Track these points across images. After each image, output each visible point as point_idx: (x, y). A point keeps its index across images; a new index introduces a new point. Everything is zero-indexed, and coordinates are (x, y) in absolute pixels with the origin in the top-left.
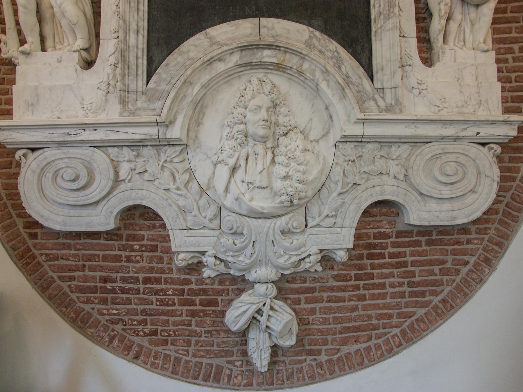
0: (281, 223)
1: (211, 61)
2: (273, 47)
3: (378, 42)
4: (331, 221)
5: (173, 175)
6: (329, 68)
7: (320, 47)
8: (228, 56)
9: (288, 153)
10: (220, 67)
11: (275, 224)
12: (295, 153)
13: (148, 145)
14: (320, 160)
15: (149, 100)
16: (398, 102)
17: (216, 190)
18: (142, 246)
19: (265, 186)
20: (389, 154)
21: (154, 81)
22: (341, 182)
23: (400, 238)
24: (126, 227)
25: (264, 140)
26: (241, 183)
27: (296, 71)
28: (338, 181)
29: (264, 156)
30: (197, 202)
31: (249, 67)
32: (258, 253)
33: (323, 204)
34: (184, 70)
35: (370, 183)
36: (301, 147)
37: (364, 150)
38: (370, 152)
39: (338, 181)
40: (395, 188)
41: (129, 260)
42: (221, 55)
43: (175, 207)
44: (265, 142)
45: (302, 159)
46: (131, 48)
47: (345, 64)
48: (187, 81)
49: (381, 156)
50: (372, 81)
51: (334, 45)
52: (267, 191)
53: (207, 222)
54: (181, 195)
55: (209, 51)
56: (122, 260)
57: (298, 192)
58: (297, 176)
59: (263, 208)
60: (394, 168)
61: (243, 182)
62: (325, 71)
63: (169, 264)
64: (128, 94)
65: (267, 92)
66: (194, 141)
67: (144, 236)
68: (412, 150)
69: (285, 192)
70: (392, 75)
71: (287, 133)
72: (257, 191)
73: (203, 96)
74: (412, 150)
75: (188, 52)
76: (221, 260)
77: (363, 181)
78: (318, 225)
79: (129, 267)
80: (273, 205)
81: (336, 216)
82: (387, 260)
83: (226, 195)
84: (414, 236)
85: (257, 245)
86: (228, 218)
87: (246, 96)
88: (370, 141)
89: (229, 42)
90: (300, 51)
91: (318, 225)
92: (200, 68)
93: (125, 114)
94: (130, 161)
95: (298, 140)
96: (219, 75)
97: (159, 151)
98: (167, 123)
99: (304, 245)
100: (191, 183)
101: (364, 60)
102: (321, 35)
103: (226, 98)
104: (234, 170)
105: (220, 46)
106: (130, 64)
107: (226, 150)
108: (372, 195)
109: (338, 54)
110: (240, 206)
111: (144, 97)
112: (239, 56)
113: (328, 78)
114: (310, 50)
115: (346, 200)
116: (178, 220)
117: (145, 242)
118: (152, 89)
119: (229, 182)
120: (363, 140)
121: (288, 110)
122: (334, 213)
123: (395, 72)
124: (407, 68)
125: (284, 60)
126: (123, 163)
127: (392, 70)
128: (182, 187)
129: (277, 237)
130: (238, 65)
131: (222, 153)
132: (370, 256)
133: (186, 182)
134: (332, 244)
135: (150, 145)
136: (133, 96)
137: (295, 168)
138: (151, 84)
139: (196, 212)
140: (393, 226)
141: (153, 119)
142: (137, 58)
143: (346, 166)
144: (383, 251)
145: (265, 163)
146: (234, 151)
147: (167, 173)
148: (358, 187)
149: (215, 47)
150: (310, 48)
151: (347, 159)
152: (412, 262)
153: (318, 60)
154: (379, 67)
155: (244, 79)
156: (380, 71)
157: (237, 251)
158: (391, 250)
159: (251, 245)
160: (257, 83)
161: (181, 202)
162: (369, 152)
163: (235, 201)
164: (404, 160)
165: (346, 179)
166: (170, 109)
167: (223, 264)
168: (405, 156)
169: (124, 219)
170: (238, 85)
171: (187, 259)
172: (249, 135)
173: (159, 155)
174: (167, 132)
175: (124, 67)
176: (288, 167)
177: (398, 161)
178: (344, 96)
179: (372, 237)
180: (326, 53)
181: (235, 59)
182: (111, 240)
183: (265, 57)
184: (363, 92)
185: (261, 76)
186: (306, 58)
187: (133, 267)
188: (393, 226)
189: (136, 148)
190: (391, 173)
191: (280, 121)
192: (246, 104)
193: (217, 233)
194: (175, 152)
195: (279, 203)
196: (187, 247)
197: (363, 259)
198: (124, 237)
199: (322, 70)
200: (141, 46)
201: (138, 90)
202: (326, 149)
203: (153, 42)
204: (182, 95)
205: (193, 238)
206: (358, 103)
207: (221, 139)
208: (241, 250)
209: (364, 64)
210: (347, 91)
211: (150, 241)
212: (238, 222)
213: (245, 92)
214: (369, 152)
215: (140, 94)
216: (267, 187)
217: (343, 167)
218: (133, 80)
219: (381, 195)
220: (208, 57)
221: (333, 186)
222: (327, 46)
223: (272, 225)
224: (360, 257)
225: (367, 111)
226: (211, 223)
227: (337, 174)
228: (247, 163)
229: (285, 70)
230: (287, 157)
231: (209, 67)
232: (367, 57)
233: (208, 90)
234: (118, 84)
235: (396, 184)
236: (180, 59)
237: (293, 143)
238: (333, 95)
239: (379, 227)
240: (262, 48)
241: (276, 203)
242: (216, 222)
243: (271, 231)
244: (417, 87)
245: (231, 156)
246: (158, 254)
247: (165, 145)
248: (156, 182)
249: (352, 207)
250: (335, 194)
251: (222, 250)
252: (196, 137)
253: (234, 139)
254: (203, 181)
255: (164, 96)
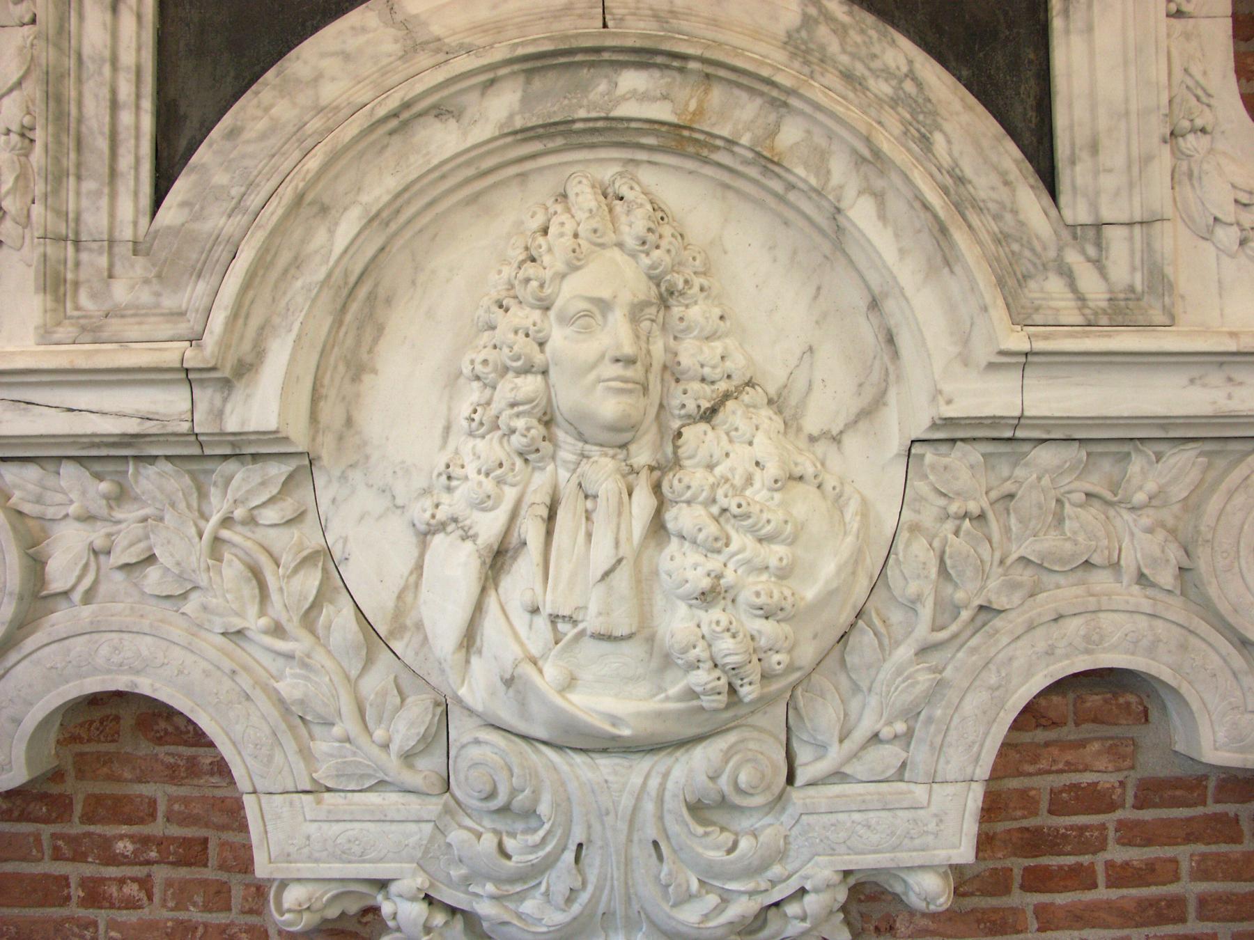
0: (691, 769)
1: (405, 115)
2: (659, 60)
3: (1077, 42)
4: (889, 755)
5: (256, 574)
6: (887, 145)
7: (844, 59)
8: (474, 96)
9: (720, 493)
10: (442, 141)
11: (666, 776)
12: (748, 493)
13: (156, 457)
14: (848, 518)
15: (159, 276)
16: (1159, 280)
17: (426, 638)
18: (145, 841)
19: (622, 630)
20: (1118, 485)
21: (180, 198)
22: (929, 603)
23: (1155, 806)
24: (83, 768)
25: (620, 437)
26: (527, 616)
27: (750, 155)
28: (918, 599)
29: (620, 503)
30: (353, 684)
31: (560, 141)
32: (599, 889)
33: (856, 688)
34: (297, 155)
35: (1046, 603)
36: (772, 470)
37: (1019, 472)
38: (1046, 481)
39: (918, 599)
40: (1143, 622)
41: (94, 895)
42: (446, 92)
43: (264, 704)
44: (624, 446)
45: (777, 517)
46: (90, 66)
47: (947, 127)
48: (310, 197)
49: (1088, 495)
50: (1053, 193)
51: (901, 53)
52: (631, 651)
53: (392, 764)
54: (289, 657)
55: (396, 78)
56: (68, 898)
57: (759, 653)
58: (755, 588)
59: (615, 720)
60: (1139, 543)
61: (535, 611)
62: (866, 153)
63: (251, 912)
64: (77, 250)
65: (631, 243)
66: (341, 438)
67: (153, 803)
68: (1209, 466)
69: (705, 655)
70: (1135, 170)
71: (714, 411)
72: (591, 648)
73: (375, 257)
74: (1209, 466)
75: (317, 79)
76: (453, 911)
77: (1016, 598)
78: (838, 776)
79: (95, 924)
80: (654, 705)
81: (909, 734)
82: (1103, 893)
83: (468, 662)
84: (1210, 800)
85: (593, 858)
86: (475, 752)
87: (547, 259)
88: (1045, 436)
89: (480, 40)
90: (765, 72)
91: (838, 776)
92: (360, 146)
93: (61, 333)
94: (88, 518)
95: (760, 439)
96: (441, 171)
97: (201, 477)
98: (226, 372)
99: (781, 855)
100: (328, 610)
101: (1023, 110)
102: (850, 13)
103: (469, 263)
104: (499, 558)
105: (441, 57)
106: (84, 129)
107: (466, 478)
108: (1050, 652)
109: (919, 85)
110: (522, 705)
111: (140, 261)
112: (519, 94)
113: (879, 184)
114: (806, 70)
115: (948, 673)
116: (278, 758)
117: (158, 828)
118: (174, 231)
119: (479, 608)
120: (1020, 434)
121: (717, 312)
122: (900, 727)
123: (1147, 160)
124: (1191, 143)
125: (700, 112)
126: (63, 523)
127: (1135, 153)
128: (293, 626)
129: (674, 828)
130: (515, 133)
131: (449, 489)
132: (1037, 880)
133: (307, 605)
134: (894, 849)
135: (167, 458)
136: (96, 261)
137: (746, 555)
138: (170, 212)
139: (348, 724)
140: (1128, 763)
141: (170, 354)
142: (114, 105)
143: (951, 536)
144: (1085, 859)
145: (623, 536)
146: (500, 482)
147: (232, 569)
148: (998, 622)
149: (424, 60)
150: (806, 63)
151: (954, 508)
152: (1202, 901)
153: (839, 110)
154: (1082, 135)
155: (542, 188)
156: (1085, 155)
157: (512, 880)
158: (1118, 854)
159: (569, 856)
160: (593, 205)
161: (290, 686)
162: (1039, 479)
163: (501, 688)
164: (1176, 508)
165: (949, 589)
166: (238, 313)
167: (459, 924)
168: (1179, 492)
169: (75, 739)
170: (518, 210)
171: (318, 905)
172: (559, 419)
173: (202, 494)
174: (229, 407)
175: (59, 142)
176: (719, 552)
177: (1150, 511)
178: (944, 255)
179: (1044, 805)
180: (871, 82)
181: (502, 107)
182: (24, 817)
183: (624, 98)
184: (1019, 240)
185: (607, 173)
186: (794, 102)
187: (113, 924)
188: (1128, 763)
189: (110, 467)
190: (1128, 561)
191: (686, 360)
192: (548, 291)
193: (433, 807)
194: (263, 484)
195: (681, 698)
196: (317, 861)
197: (1007, 891)
198: (78, 809)
199: (854, 151)
200: (127, 58)
201: (117, 235)
202: (870, 471)
203: (182, 44)
204: (285, 258)
205: (337, 828)
206: (1001, 283)
207: (447, 429)
208: (531, 874)
209: (1020, 125)
210: (960, 237)
211: (180, 824)
212: (516, 770)
213: (541, 240)
214: (1039, 479)
215: (123, 250)
216: (630, 636)
217: (936, 544)
218: (98, 194)
219: (1088, 652)
220: (393, 102)
221: (896, 616)
222: (874, 56)
223: (654, 783)
224: (998, 883)
225: (1038, 318)
226: (411, 766)
227: (915, 571)
228: (549, 533)
229: (705, 152)
230: (715, 510)
231: (396, 141)
232: (1031, 101)
233: (396, 234)
234: (37, 210)
235: (1146, 606)
236: (284, 111)
237: (741, 451)
238: (902, 252)
239: (1071, 768)
240: (612, 63)
241: (667, 699)
242: (430, 764)
243: (649, 807)
244: (1231, 219)
245: (484, 504)
246: (209, 873)
247: (226, 457)
248: (191, 606)
249: (971, 705)
250: (904, 652)
251: (456, 873)
252: (349, 422)
253: (499, 433)
254: (378, 604)
255: (212, 258)
